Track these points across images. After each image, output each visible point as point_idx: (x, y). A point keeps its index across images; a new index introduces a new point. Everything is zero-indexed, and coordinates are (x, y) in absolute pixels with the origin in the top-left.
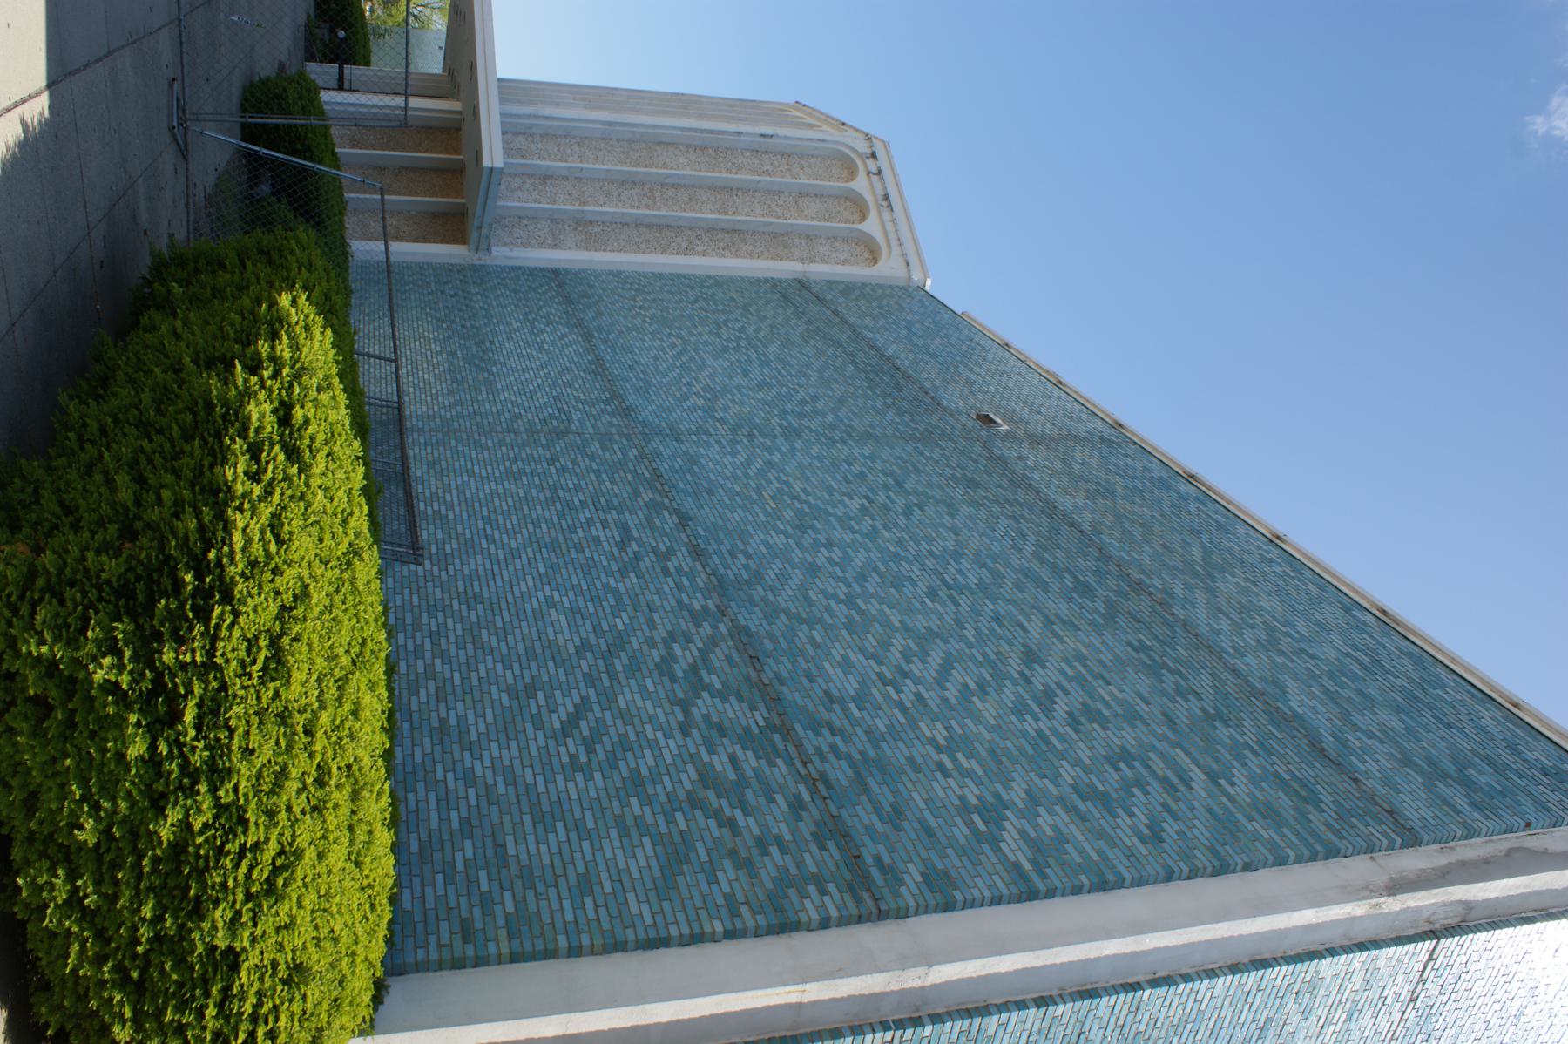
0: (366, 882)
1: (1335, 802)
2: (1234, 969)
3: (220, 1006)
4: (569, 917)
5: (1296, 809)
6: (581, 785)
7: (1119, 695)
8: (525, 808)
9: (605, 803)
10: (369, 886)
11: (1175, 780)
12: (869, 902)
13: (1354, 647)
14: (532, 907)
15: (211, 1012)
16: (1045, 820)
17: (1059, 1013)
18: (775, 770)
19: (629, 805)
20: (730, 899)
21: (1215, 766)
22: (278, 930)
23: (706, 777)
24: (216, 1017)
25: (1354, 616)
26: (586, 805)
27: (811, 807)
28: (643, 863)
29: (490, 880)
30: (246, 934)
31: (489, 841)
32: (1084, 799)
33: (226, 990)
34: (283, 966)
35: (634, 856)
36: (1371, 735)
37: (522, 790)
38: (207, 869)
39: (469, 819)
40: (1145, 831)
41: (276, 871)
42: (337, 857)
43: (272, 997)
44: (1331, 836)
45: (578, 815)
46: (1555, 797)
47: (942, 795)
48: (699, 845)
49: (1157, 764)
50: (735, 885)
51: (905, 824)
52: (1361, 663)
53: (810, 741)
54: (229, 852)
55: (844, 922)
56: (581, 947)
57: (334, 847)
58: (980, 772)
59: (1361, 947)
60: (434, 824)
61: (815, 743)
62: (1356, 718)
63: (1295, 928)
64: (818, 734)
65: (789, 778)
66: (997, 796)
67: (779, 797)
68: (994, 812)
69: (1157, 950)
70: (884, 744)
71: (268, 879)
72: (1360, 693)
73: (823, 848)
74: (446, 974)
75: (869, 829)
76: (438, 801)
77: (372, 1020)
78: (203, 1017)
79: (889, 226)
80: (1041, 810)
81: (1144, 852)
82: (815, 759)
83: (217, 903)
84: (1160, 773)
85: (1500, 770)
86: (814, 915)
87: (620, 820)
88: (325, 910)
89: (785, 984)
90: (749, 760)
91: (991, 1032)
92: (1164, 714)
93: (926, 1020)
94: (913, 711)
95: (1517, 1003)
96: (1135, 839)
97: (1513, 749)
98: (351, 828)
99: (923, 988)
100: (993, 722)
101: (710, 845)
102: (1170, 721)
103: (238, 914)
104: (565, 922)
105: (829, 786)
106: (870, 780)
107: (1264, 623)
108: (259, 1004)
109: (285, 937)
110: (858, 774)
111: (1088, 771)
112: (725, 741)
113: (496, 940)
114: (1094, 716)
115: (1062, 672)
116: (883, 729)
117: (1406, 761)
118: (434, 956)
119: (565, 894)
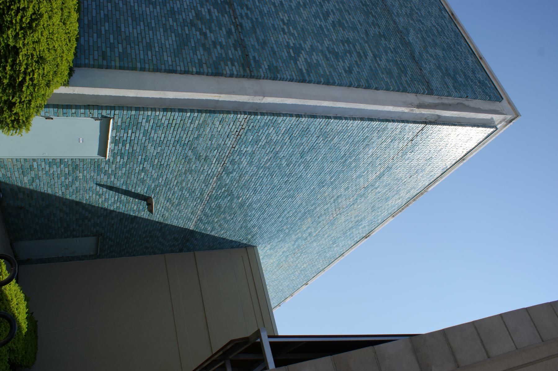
0: (67, 31)
1: (412, 75)
2: (362, 119)
3: (12, 66)
4: (142, 57)
5: (398, 73)
6: (152, 10)
7: (352, 20)
8: (130, 15)
9: (160, 18)
10: (69, 33)
11: (362, 54)
12: (248, 71)
13: (438, 24)
14: (129, 51)
15: (8, 68)
16: (314, 57)
17: (303, 120)
18: (224, 18)
19: (169, 21)
20: (200, 60)
21: (377, 53)
22: (33, 43)
23: (198, 16)
24: (10, 70)
25: (442, 13)
26: (152, 17)
27: (235, 34)
28: (171, 43)
29: (114, 39)
30: (21, 42)
31: (115, 25)
32: (330, 52)
33: (14, 61)
34: (35, 56)
35: (168, 40)
36: (431, 56)
37: (129, 7)
38: (4, 14)
39: (108, 15)
40: (347, 69)
41: (32, 20)
42: (56, 19)
43: (32, 66)
44: (406, 85)
45: (149, 21)
46: (479, 90)
47: (281, 40)
48: (192, 40)
49: (358, 47)
50: (203, 56)
51: (266, 48)
52: (438, 30)
53: (238, 10)
54: (12, 9)
55: (238, 76)
56: (145, 68)
57: (55, 15)
58: (296, 35)
59: (403, 121)
60: (94, 14)
61: (240, 11)
62: (429, 49)
63: (385, 111)
64: (242, 8)
65: (228, 23)
66: (300, 45)
67: (223, 29)
68: (298, 50)
69: (339, 108)
70: (265, 18)
71: (29, 23)
72: (433, 40)
73: (236, 50)
74: (96, 71)
75: (253, 46)
76: (96, 6)
77: (68, 81)
78: (6, 69)
80: (314, 53)
81: (345, 76)
82: (239, 17)
83: (9, 28)
84: (358, 51)
85: (466, 77)
86: (228, 72)
87: (164, 25)
88: (51, 39)
89: (214, 93)
90: (215, 13)
91: (279, 122)
92: (366, 30)
93: (259, 114)
94: (278, 8)
95: (440, 147)
96: (343, 71)
97: (473, 72)
98: (62, 9)
99: (260, 103)
100: (305, 18)
101: (196, 40)
102: (367, 33)
103: (17, 34)
104: (140, 59)
105: (242, 28)
106: (257, 29)
107: (411, 7)
108: (26, 69)
109: (36, 46)
110: (253, 26)
111: (334, 43)
112: (208, 4)
113: (115, 61)
114: (341, 25)
115: (335, 6)
116: (266, 12)
117: (439, 67)
118: (92, 63)
119: (141, 49)
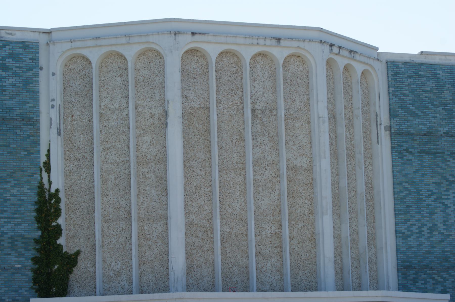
79: (362, 59)
